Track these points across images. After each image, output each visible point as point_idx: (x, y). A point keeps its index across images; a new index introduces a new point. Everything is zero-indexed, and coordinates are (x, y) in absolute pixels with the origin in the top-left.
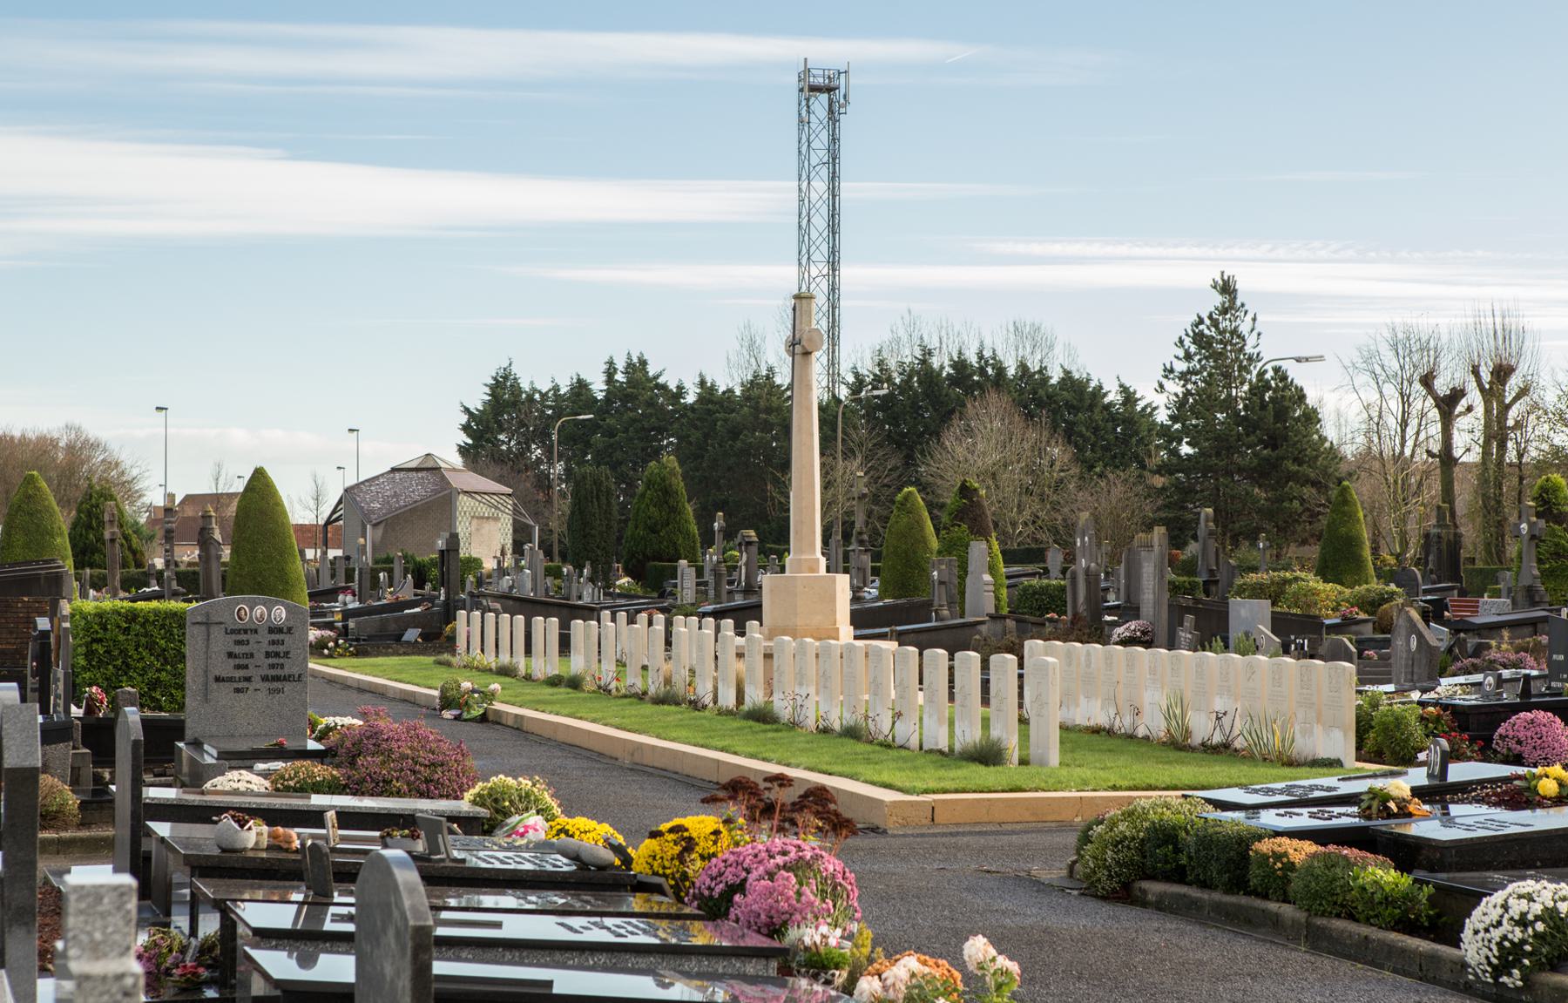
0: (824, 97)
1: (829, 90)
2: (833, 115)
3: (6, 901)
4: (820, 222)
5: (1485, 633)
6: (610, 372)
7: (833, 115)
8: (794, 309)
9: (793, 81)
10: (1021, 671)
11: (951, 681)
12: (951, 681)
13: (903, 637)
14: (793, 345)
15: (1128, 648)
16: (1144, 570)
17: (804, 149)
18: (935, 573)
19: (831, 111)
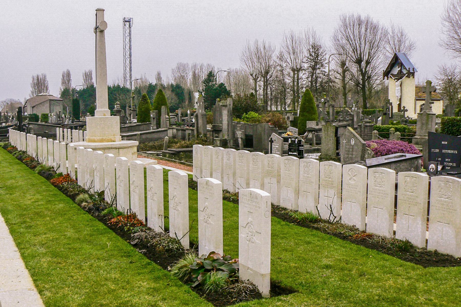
0: (128, 23)
1: (129, 22)
2: (130, 27)
3: (36, 200)
4: (128, 47)
5: (318, 131)
6: (67, 77)
7: (130, 27)
8: (96, 15)
9: (122, 21)
10: (38, 169)
11: (145, 177)
12: (145, 177)
13: (123, 138)
14: (96, 28)
15: (205, 146)
16: (224, 113)
17: (124, 40)
18: (152, 115)
19: (129, 26)
